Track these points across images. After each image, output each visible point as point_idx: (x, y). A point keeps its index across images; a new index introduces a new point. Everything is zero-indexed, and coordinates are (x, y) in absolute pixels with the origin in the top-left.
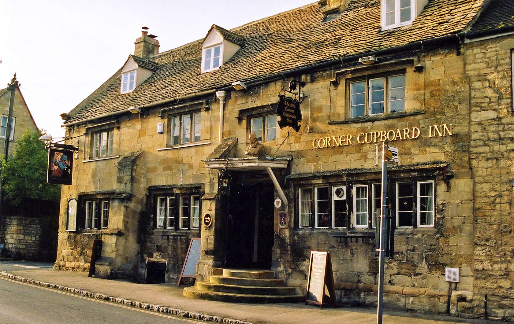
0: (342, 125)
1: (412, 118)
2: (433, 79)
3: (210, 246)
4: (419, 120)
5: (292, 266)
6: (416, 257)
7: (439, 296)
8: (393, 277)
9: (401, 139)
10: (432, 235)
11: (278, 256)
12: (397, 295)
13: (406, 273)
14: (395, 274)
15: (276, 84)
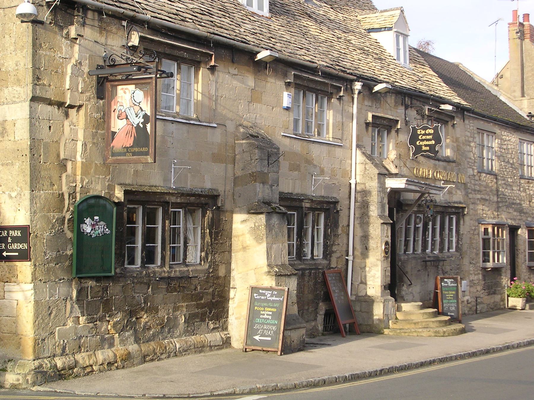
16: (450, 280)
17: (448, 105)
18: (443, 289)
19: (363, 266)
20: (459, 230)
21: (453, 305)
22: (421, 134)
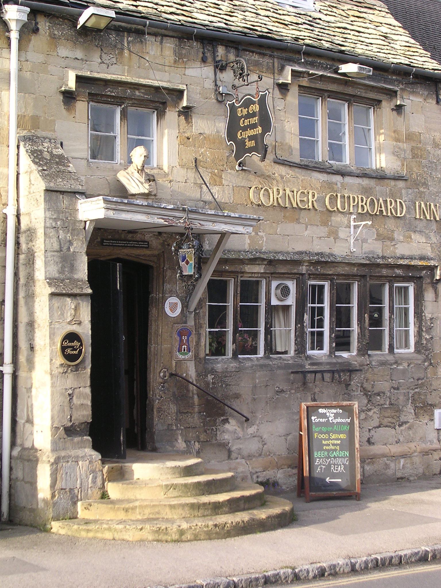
0: (297, 170)
1: (392, 183)
2: (414, 130)
3: (79, 413)
4: (401, 189)
5: (203, 437)
6: (401, 398)
7: (432, 451)
8: (372, 432)
9: (385, 214)
10: (420, 364)
11: (170, 420)
12: (385, 459)
13: (389, 424)
14: (375, 428)
15: (161, 43)
16: (334, 411)
17: (350, 63)
18: (314, 429)
19: (29, 386)
20: (422, 312)
21: (339, 461)
22: (242, 117)
